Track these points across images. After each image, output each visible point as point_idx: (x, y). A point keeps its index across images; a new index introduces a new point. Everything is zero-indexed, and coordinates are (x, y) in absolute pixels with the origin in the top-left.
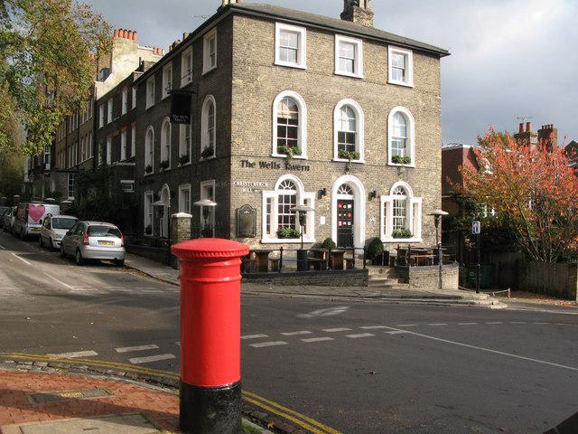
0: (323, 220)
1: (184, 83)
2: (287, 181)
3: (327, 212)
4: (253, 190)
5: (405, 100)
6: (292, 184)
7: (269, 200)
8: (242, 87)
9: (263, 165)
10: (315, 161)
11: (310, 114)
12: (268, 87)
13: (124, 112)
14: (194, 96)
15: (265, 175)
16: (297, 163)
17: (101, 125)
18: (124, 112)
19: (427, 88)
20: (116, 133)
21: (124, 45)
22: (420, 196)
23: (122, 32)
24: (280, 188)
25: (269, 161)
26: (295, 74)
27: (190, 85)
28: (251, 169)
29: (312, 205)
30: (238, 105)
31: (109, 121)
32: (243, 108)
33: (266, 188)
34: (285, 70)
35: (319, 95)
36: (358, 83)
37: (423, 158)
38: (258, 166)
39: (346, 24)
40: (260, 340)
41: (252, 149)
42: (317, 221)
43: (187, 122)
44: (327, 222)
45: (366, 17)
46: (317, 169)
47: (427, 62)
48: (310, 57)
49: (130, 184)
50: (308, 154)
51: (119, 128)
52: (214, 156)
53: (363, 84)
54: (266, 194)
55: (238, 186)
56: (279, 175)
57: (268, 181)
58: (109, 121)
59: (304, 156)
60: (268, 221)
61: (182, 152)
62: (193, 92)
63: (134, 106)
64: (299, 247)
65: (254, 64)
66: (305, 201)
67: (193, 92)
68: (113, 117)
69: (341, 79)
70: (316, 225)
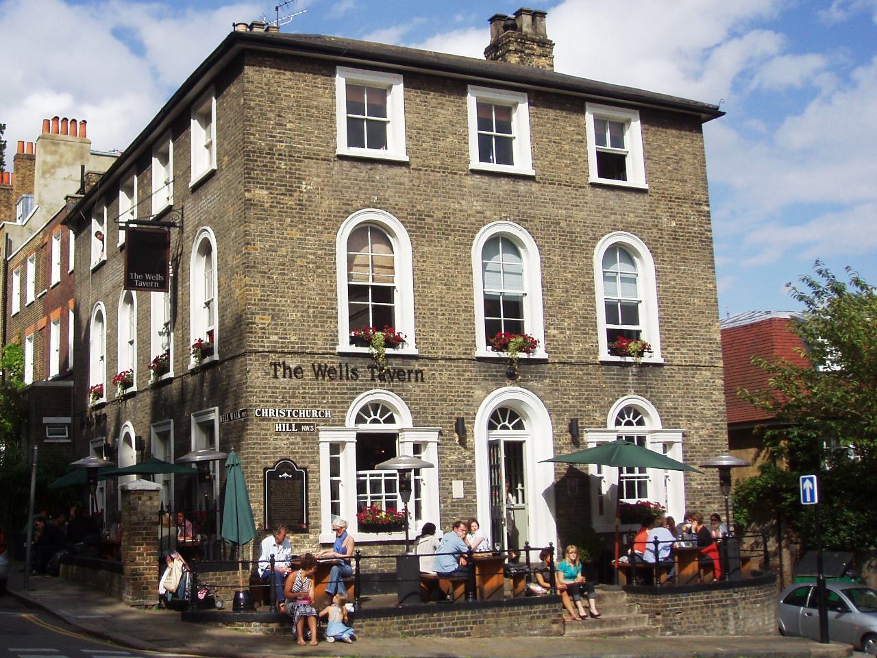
0: (458, 489)
1: (158, 205)
2: (375, 406)
3: (465, 471)
4: (298, 426)
5: (631, 218)
6: (385, 410)
7: (335, 448)
8: (267, 205)
9: (321, 372)
10: (435, 359)
11: (418, 256)
12: (327, 204)
13: (56, 277)
14: (174, 233)
15: (323, 394)
16: (396, 364)
17: (16, 308)
18: (56, 277)
19: (678, 189)
20: (42, 322)
21: (63, 148)
22: (677, 426)
23: (413, 375)
24: (359, 420)
25: (332, 362)
26: (380, 173)
27: (169, 209)
28: (295, 381)
29: (430, 454)
30: (259, 245)
31: (31, 297)
32: (273, 250)
33: (326, 422)
34: (359, 165)
35: (439, 214)
36: (522, 187)
37: (680, 342)
38: (309, 375)
39: (497, 66)
40: (372, 478)
41: (293, 339)
42: (445, 491)
43: (162, 287)
44: (466, 492)
45: (538, 50)
46: (440, 375)
47: (673, 140)
48: (413, 134)
49: (63, 425)
50: (649, 174)
51: (46, 313)
52: (216, 357)
53: (535, 187)
54: (327, 436)
55: (264, 419)
56: (355, 392)
57: (332, 406)
58: (31, 297)
59: (409, 348)
60: (335, 494)
61: (156, 351)
62: (174, 225)
63: (72, 267)
64: (401, 550)
65: (291, 156)
66: (417, 448)
67: (174, 225)
68: (36, 292)
69: (486, 179)
70: (443, 500)
